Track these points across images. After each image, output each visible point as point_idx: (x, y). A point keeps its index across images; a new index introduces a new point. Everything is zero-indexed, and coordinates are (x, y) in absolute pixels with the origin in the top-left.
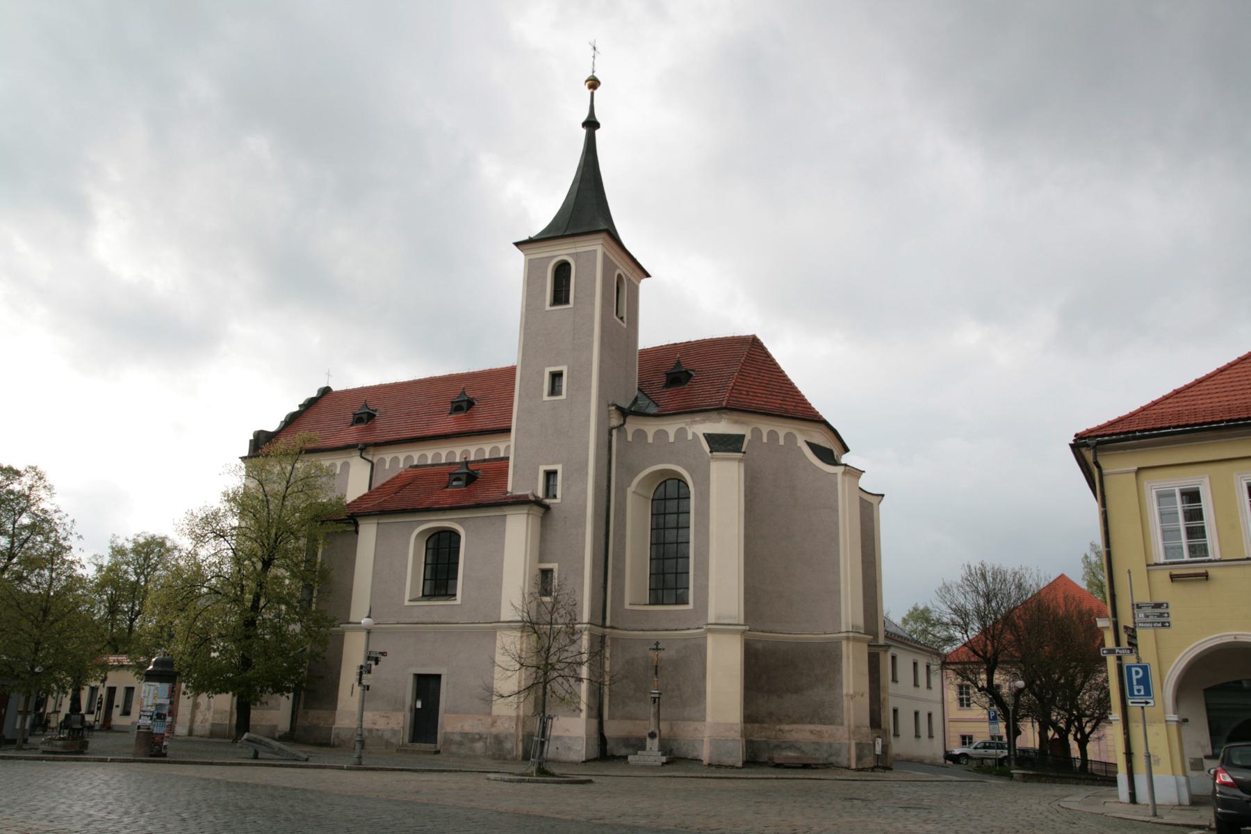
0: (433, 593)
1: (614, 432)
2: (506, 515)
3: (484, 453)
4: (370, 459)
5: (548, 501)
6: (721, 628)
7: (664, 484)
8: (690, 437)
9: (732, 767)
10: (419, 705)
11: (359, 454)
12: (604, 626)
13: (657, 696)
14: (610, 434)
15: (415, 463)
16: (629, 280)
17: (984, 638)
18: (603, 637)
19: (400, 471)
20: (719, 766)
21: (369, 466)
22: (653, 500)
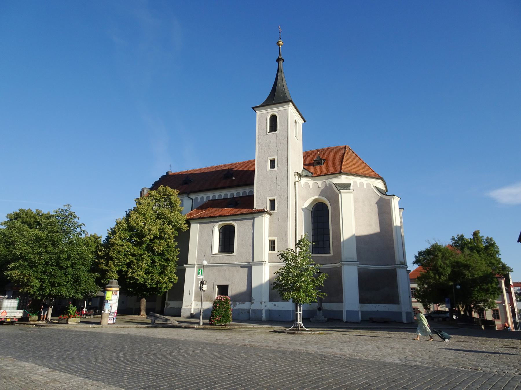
0: (223, 251)
1: (297, 183)
3: (216, 197)
6: (350, 262)
9: (357, 323)
11: (187, 196)
14: (295, 184)
15: (211, 199)
17: (212, 310)
19: (204, 202)
20: (351, 323)
21: (191, 201)
22: (312, 211)
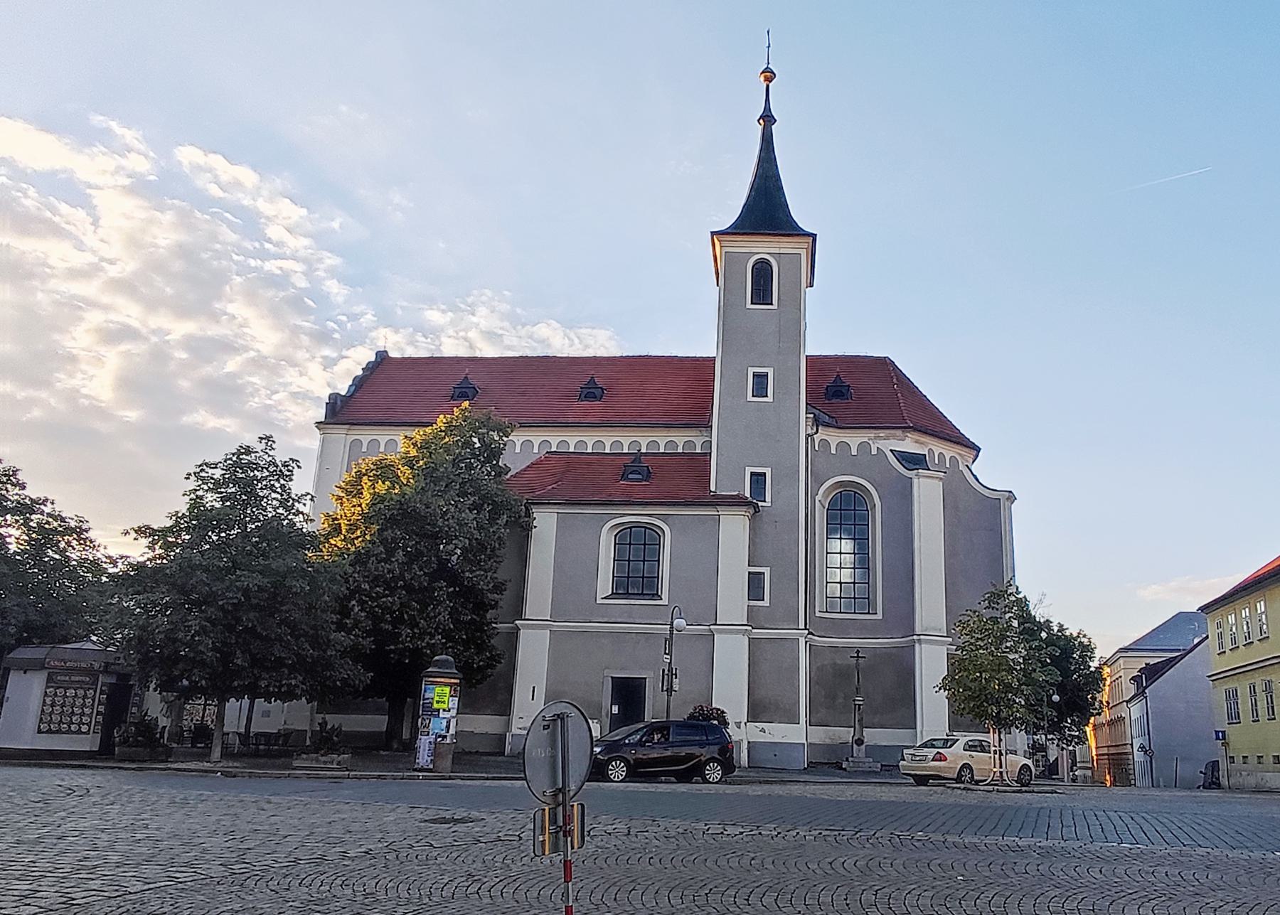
8: (874, 452)
10: (615, 709)
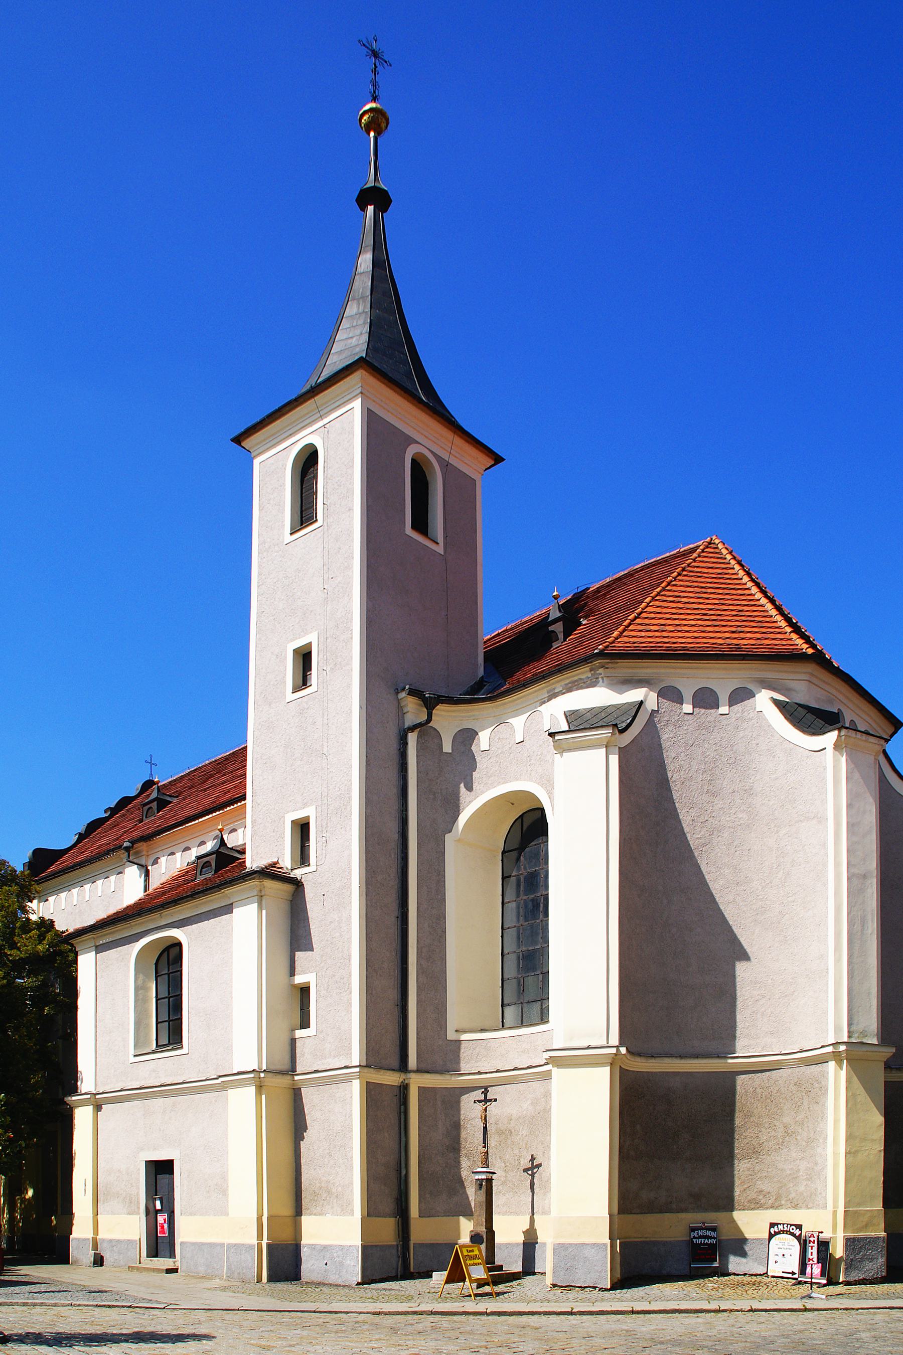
1: (412, 738)
2: (232, 904)
4: (143, 863)
5: (298, 873)
7: (520, 819)
12: (403, 1066)
13: (484, 1177)
16: (446, 466)
18: (404, 1089)
22: (503, 853)
